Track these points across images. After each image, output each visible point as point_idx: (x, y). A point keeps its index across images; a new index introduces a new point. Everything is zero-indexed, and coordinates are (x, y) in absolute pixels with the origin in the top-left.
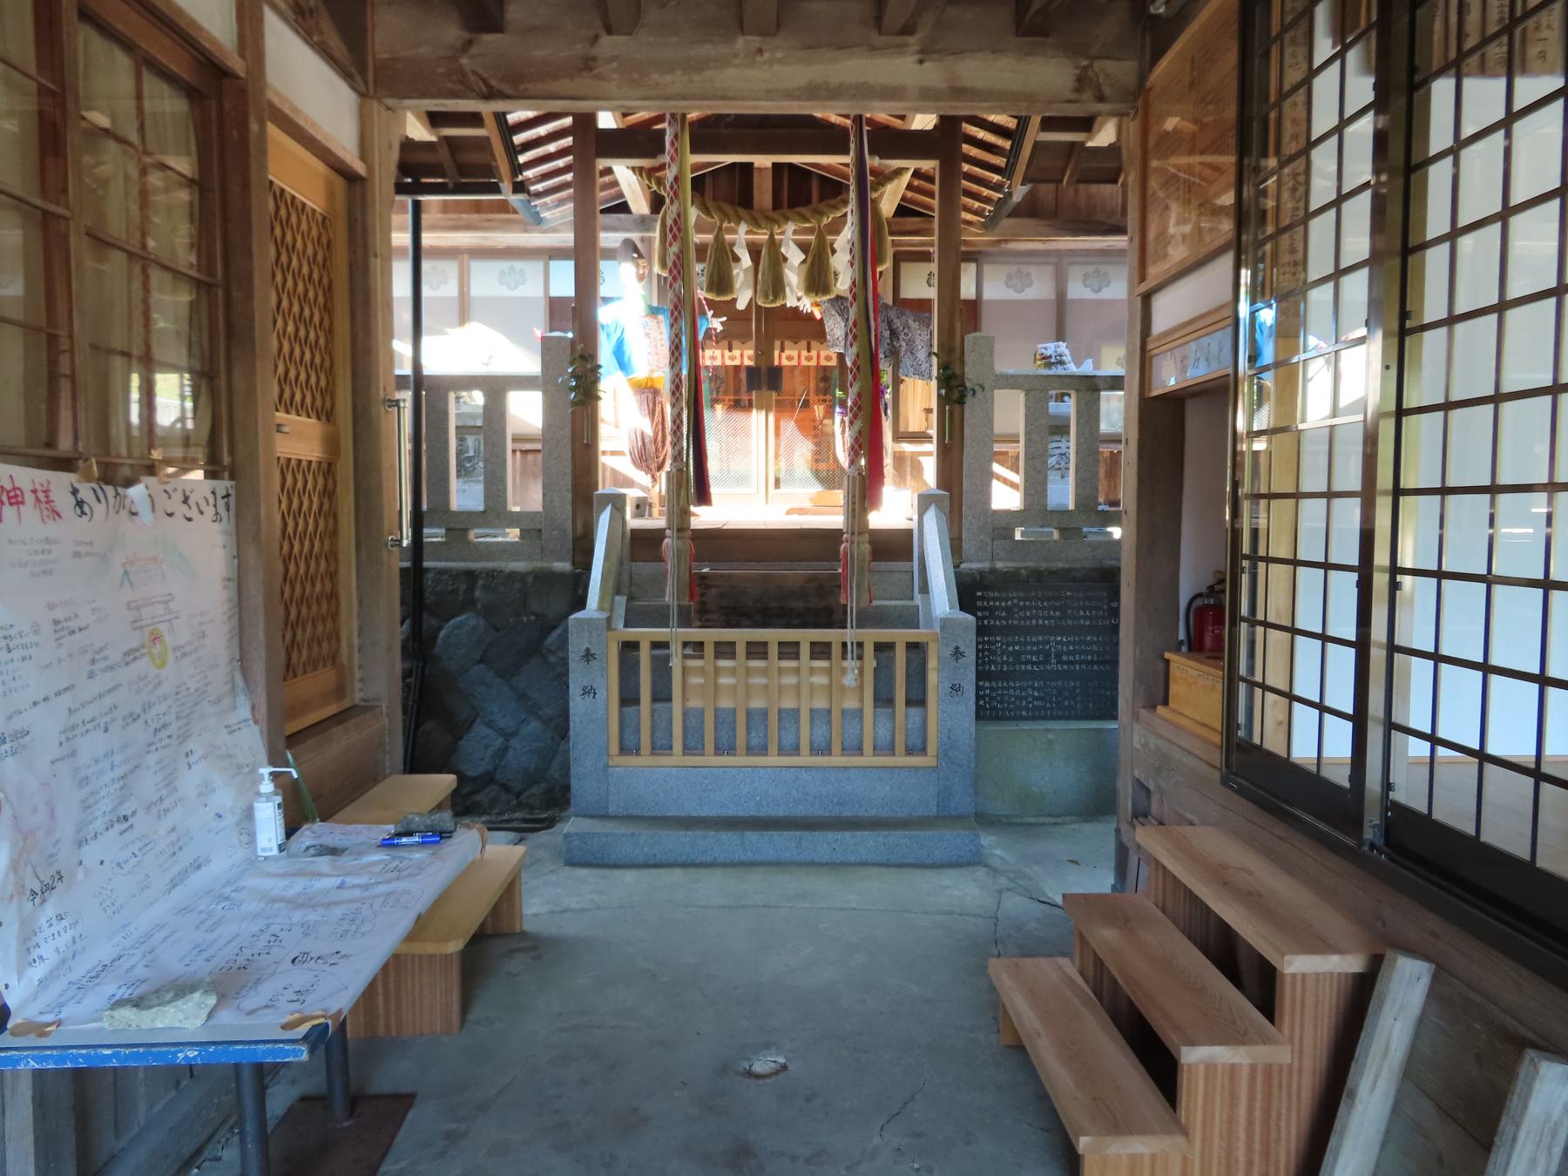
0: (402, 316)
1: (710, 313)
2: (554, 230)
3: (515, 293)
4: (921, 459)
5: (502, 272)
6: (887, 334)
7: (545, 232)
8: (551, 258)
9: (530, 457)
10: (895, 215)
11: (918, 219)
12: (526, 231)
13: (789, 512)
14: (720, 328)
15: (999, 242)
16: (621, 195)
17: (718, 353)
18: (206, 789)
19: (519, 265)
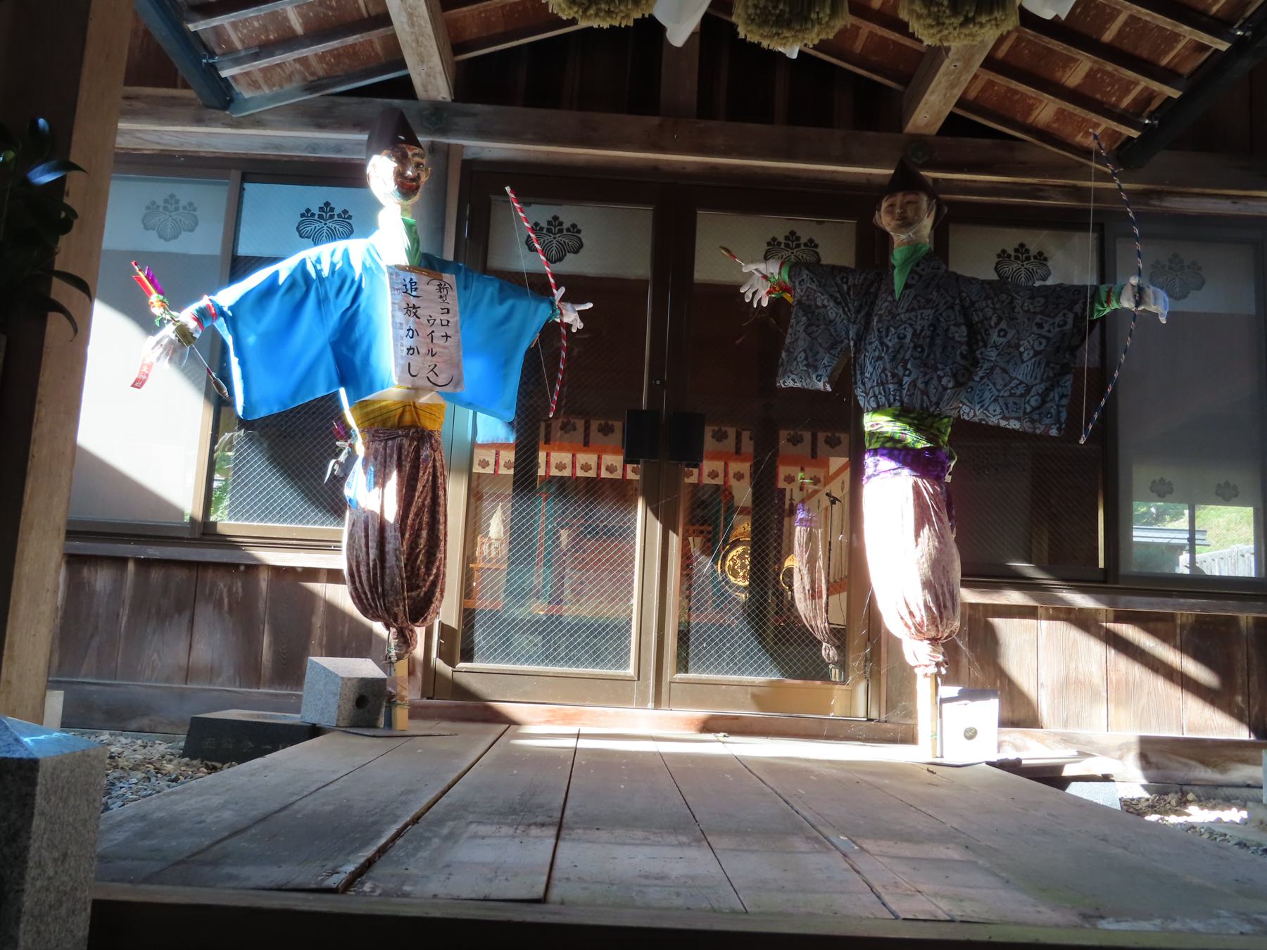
0: (933, 790)
1: (559, 293)
2: (256, 122)
3: (173, 247)
4: (998, 622)
5: (152, 207)
6: (961, 333)
7: (238, 124)
8: (245, 178)
9: (156, 575)
10: (944, 131)
11: (987, 142)
12: (199, 121)
13: (708, 726)
14: (578, 325)
15: (1146, 194)
16: (393, 44)
17: (566, 457)
18: (790, 479)
19: (186, 192)
